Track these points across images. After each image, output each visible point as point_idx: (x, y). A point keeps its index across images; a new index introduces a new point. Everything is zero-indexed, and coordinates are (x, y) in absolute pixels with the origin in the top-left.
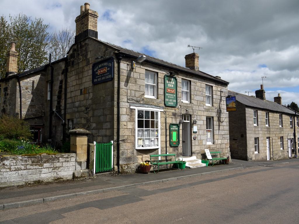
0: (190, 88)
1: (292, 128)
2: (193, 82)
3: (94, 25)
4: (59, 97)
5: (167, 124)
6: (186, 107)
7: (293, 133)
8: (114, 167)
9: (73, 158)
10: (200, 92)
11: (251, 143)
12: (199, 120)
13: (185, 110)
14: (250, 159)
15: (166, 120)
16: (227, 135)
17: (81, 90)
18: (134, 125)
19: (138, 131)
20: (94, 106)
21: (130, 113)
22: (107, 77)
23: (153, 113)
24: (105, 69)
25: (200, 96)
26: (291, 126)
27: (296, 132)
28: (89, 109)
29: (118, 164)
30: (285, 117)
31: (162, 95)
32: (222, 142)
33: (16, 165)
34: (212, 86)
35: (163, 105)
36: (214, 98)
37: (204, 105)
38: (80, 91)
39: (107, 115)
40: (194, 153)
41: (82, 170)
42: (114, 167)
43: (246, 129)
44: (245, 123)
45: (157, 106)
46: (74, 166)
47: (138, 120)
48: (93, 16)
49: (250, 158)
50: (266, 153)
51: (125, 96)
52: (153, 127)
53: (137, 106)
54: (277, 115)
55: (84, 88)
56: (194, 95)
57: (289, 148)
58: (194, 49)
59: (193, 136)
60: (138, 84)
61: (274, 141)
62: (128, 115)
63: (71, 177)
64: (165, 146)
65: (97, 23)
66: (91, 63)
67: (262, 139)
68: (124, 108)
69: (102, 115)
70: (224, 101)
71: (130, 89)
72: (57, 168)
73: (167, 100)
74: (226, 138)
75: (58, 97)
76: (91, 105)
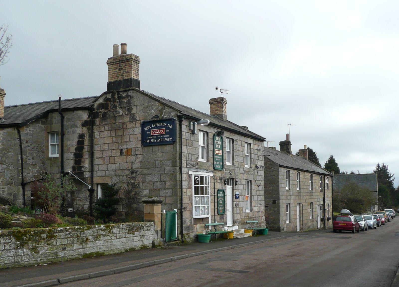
0: (233, 147)
1: (321, 191)
2: (235, 140)
3: (137, 73)
4: (78, 156)
5: (215, 190)
6: (230, 169)
7: (322, 198)
8: (178, 236)
9: (152, 226)
10: (241, 151)
11: (283, 209)
12: (240, 185)
13: (229, 174)
14: (282, 230)
15: (214, 186)
16: (263, 201)
17: (121, 150)
18: (191, 192)
19: (195, 197)
20: (145, 171)
21: (188, 179)
22: (166, 140)
23: (202, 178)
24: (162, 130)
25: (241, 156)
26: (321, 189)
27: (326, 196)
28: (136, 173)
29: (181, 233)
30: (315, 177)
31: (212, 157)
32: (259, 210)
33: (120, 233)
34: (250, 144)
35: (212, 169)
36: (252, 158)
37: (244, 167)
38: (119, 151)
39: (166, 181)
40: (236, 222)
41: (158, 239)
42: (178, 236)
43: (279, 194)
44: (278, 186)
45: (208, 170)
46: (153, 234)
47: (195, 186)
48: (136, 61)
49: (282, 228)
50: (296, 222)
51: (185, 160)
52: (202, 193)
53: (194, 171)
54: (308, 175)
55: (127, 148)
56: (236, 156)
57: (318, 217)
58: (222, 93)
59: (235, 203)
60: (194, 147)
61: (304, 209)
62: (187, 181)
63: (151, 246)
64: (214, 215)
65: (139, 69)
66: (138, 119)
67: (293, 206)
68: (184, 173)
69: (159, 181)
70: (260, 160)
71: (188, 153)
72: (143, 236)
73: (215, 163)
74: (262, 204)
75: (75, 154)
76: (139, 169)
